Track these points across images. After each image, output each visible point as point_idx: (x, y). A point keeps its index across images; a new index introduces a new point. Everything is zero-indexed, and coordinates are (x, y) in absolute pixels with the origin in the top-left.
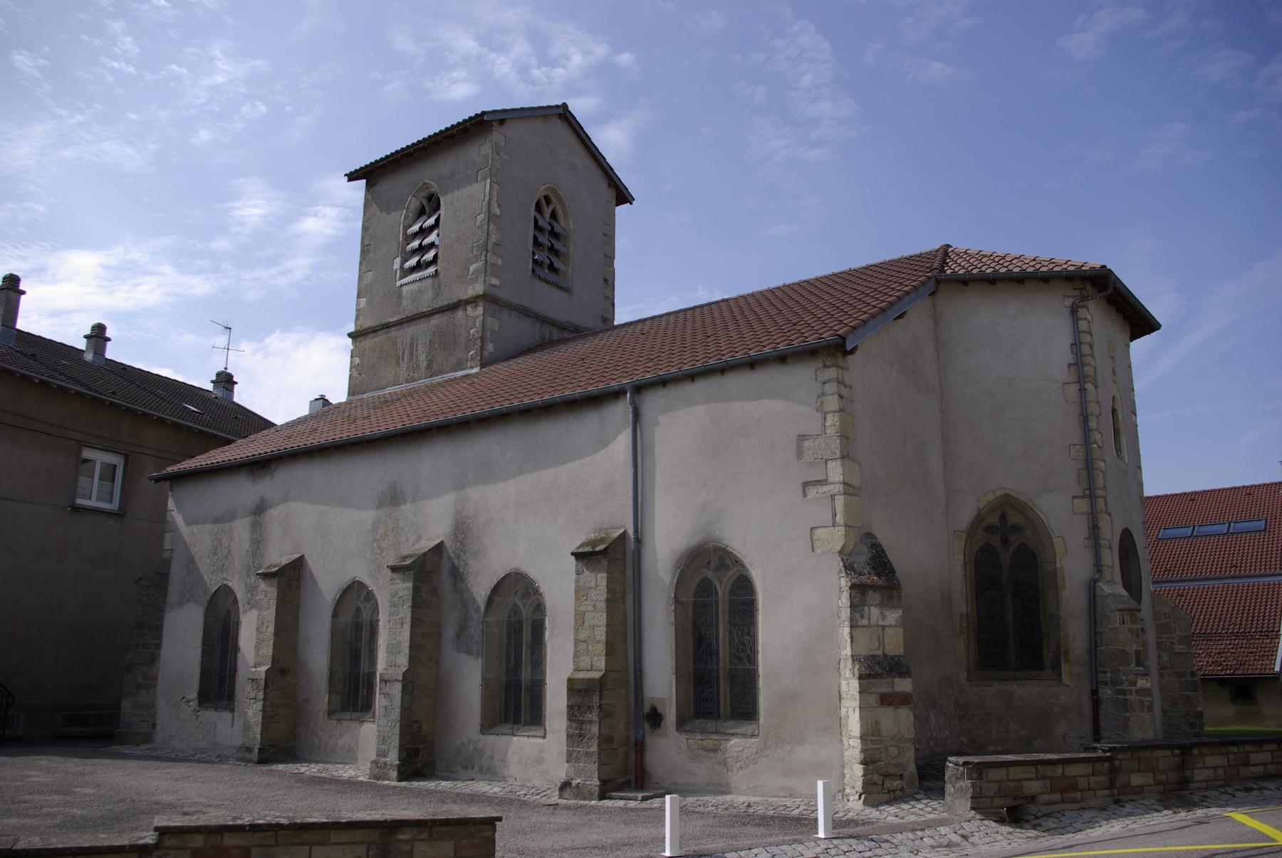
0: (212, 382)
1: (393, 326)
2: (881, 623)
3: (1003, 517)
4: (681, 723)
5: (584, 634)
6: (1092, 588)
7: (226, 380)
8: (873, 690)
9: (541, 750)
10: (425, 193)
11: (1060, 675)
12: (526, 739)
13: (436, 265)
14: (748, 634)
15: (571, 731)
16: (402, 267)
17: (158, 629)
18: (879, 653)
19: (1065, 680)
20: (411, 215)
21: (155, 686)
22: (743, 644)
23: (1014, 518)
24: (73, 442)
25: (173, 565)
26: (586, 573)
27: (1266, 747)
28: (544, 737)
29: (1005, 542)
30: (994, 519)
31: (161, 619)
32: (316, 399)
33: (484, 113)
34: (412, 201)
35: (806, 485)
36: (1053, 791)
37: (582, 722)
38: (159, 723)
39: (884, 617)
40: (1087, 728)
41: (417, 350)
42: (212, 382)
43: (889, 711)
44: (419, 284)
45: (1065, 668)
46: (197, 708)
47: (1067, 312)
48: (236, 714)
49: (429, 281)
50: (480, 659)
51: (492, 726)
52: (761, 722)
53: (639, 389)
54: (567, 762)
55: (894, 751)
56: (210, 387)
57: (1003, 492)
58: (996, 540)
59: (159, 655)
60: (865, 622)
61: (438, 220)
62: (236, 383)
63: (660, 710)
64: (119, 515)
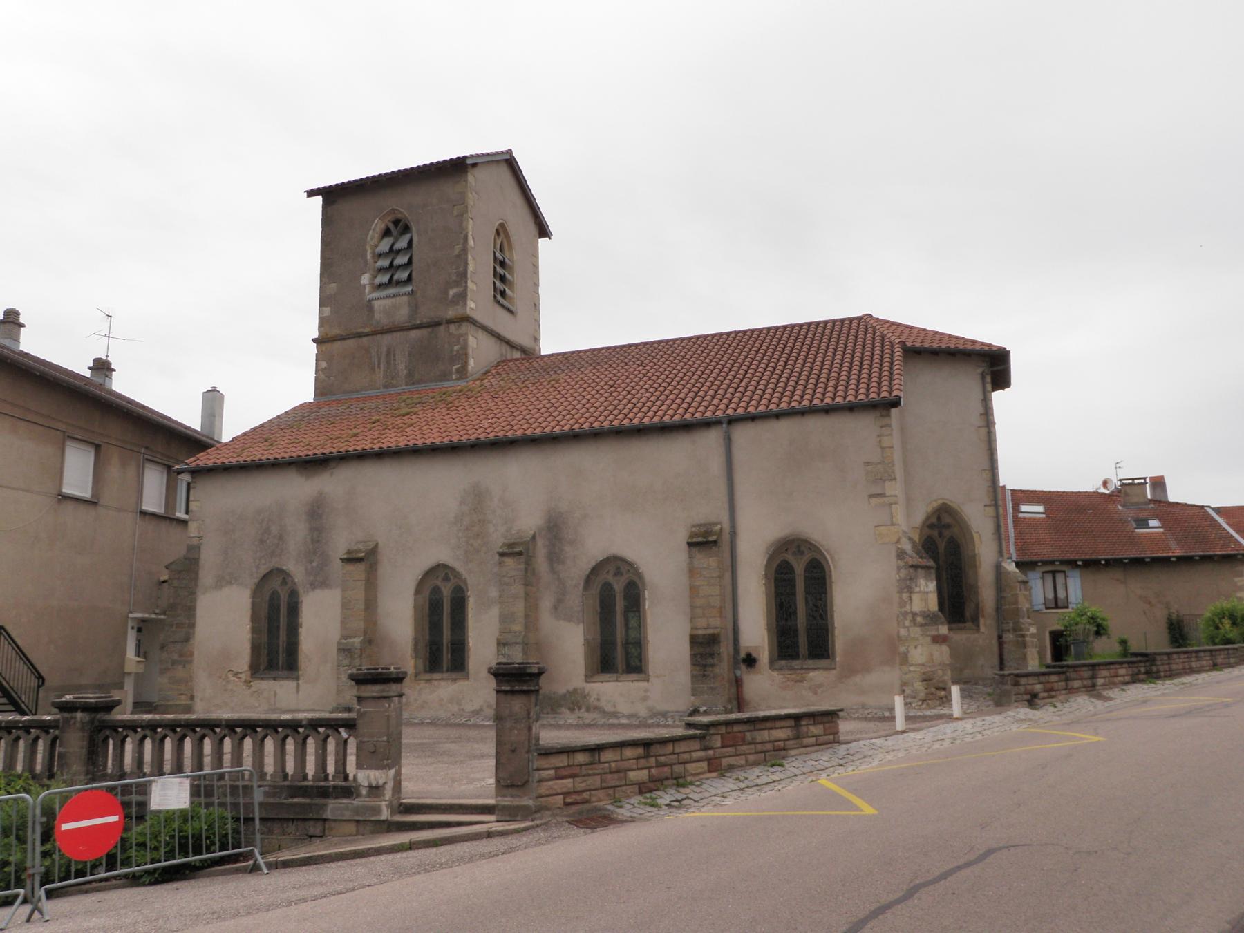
0: (89, 368)
1: (365, 336)
2: (926, 590)
3: (939, 518)
4: (772, 663)
5: (699, 602)
6: (998, 569)
7: (102, 367)
8: (928, 633)
9: (646, 691)
10: (391, 218)
11: (978, 626)
12: (630, 683)
13: (411, 284)
14: (821, 599)
15: (695, 673)
16: (372, 284)
17: (191, 610)
18: (926, 610)
19: (982, 628)
20: (376, 236)
21: (191, 662)
22: (816, 607)
23: (947, 519)
24: (59, 432)
25: (202, 550)
26: (698, 556)
27: (1124, 666)
28: (648, 681)
29: (940, 535)
30: (934, 520)
31: (194, 601)
32: (208, 391)
33: (465, 157)
34: (378, 225)
35: (871, 496)
36: (1045, 691)
37: (705, 666)
38: (198, 696)
39: (927, 586)
40: (996, 661)
41: (395, 360)
42: (89, 368)
43: (936, 647)
44: (393, 300)
45: (982, 621)
46: (249, 679)
47: (978, 378)
48: (300, 682)
49: (405, 298)
50: (581, 626)
51: (591, 676)
52: (837, 659)
53: (732, 421)
54: (693, 695)
55: (940, 672)
56: (87, 373)
57: (940, 502)
58: (935, 533)
59: (194, 633)
60: (917, 589)
61: (410, 243)
62: (115, 370)
63: (754, 655)
64: (92, 503)
